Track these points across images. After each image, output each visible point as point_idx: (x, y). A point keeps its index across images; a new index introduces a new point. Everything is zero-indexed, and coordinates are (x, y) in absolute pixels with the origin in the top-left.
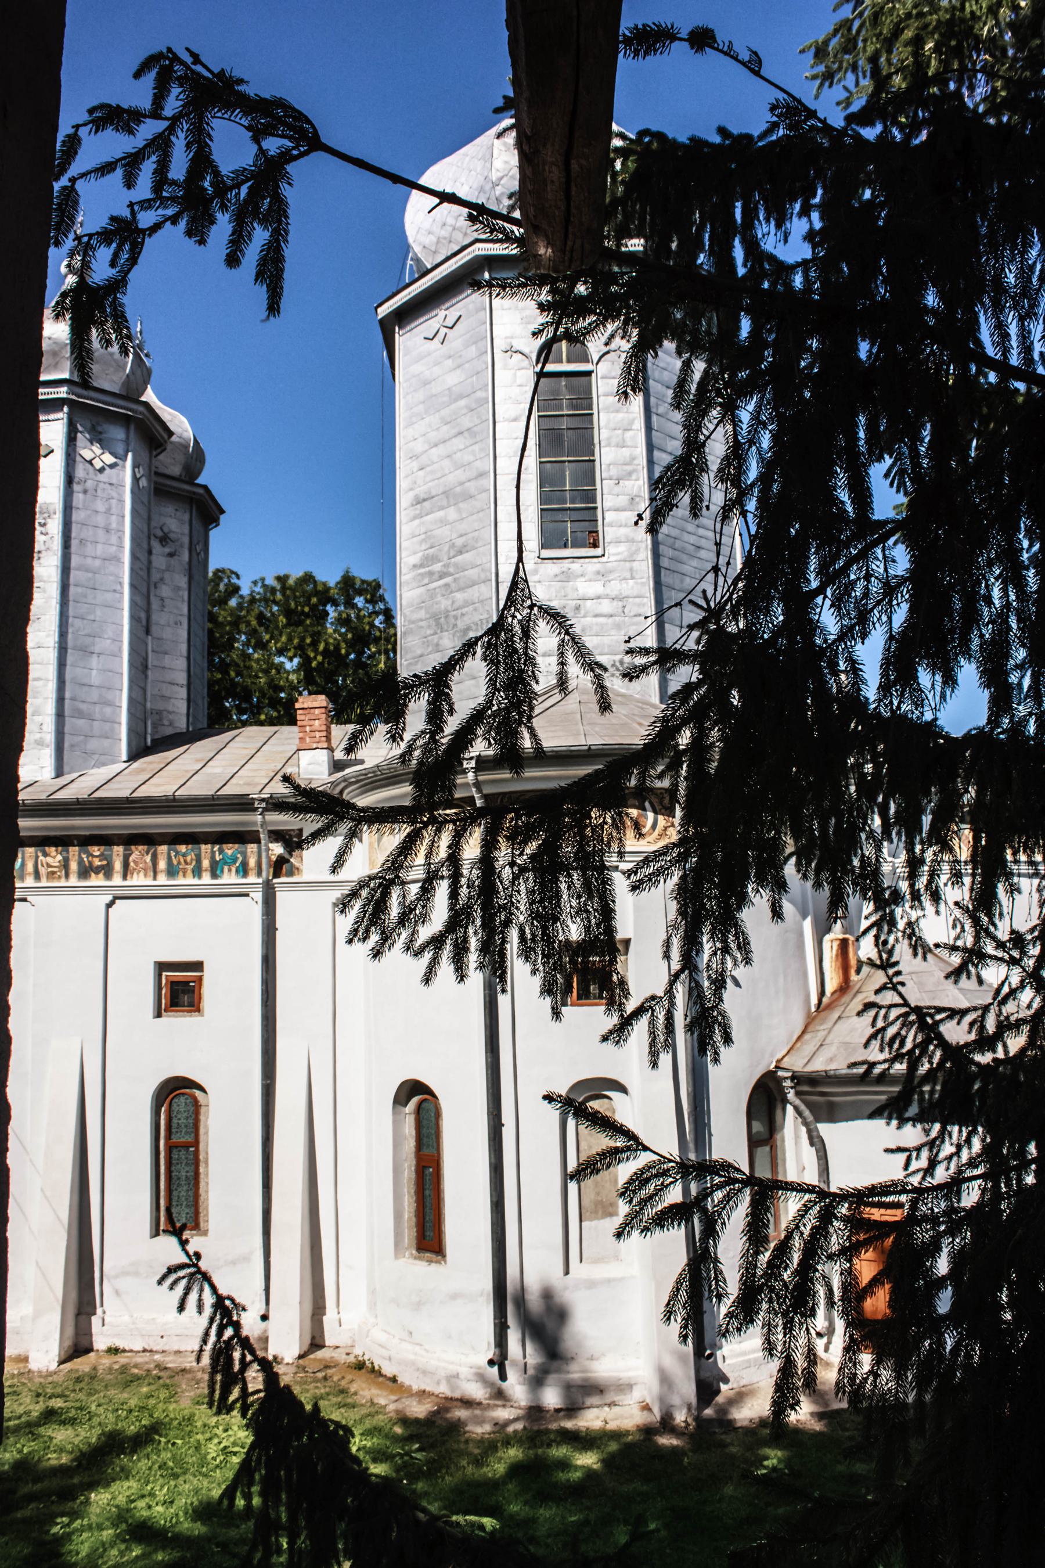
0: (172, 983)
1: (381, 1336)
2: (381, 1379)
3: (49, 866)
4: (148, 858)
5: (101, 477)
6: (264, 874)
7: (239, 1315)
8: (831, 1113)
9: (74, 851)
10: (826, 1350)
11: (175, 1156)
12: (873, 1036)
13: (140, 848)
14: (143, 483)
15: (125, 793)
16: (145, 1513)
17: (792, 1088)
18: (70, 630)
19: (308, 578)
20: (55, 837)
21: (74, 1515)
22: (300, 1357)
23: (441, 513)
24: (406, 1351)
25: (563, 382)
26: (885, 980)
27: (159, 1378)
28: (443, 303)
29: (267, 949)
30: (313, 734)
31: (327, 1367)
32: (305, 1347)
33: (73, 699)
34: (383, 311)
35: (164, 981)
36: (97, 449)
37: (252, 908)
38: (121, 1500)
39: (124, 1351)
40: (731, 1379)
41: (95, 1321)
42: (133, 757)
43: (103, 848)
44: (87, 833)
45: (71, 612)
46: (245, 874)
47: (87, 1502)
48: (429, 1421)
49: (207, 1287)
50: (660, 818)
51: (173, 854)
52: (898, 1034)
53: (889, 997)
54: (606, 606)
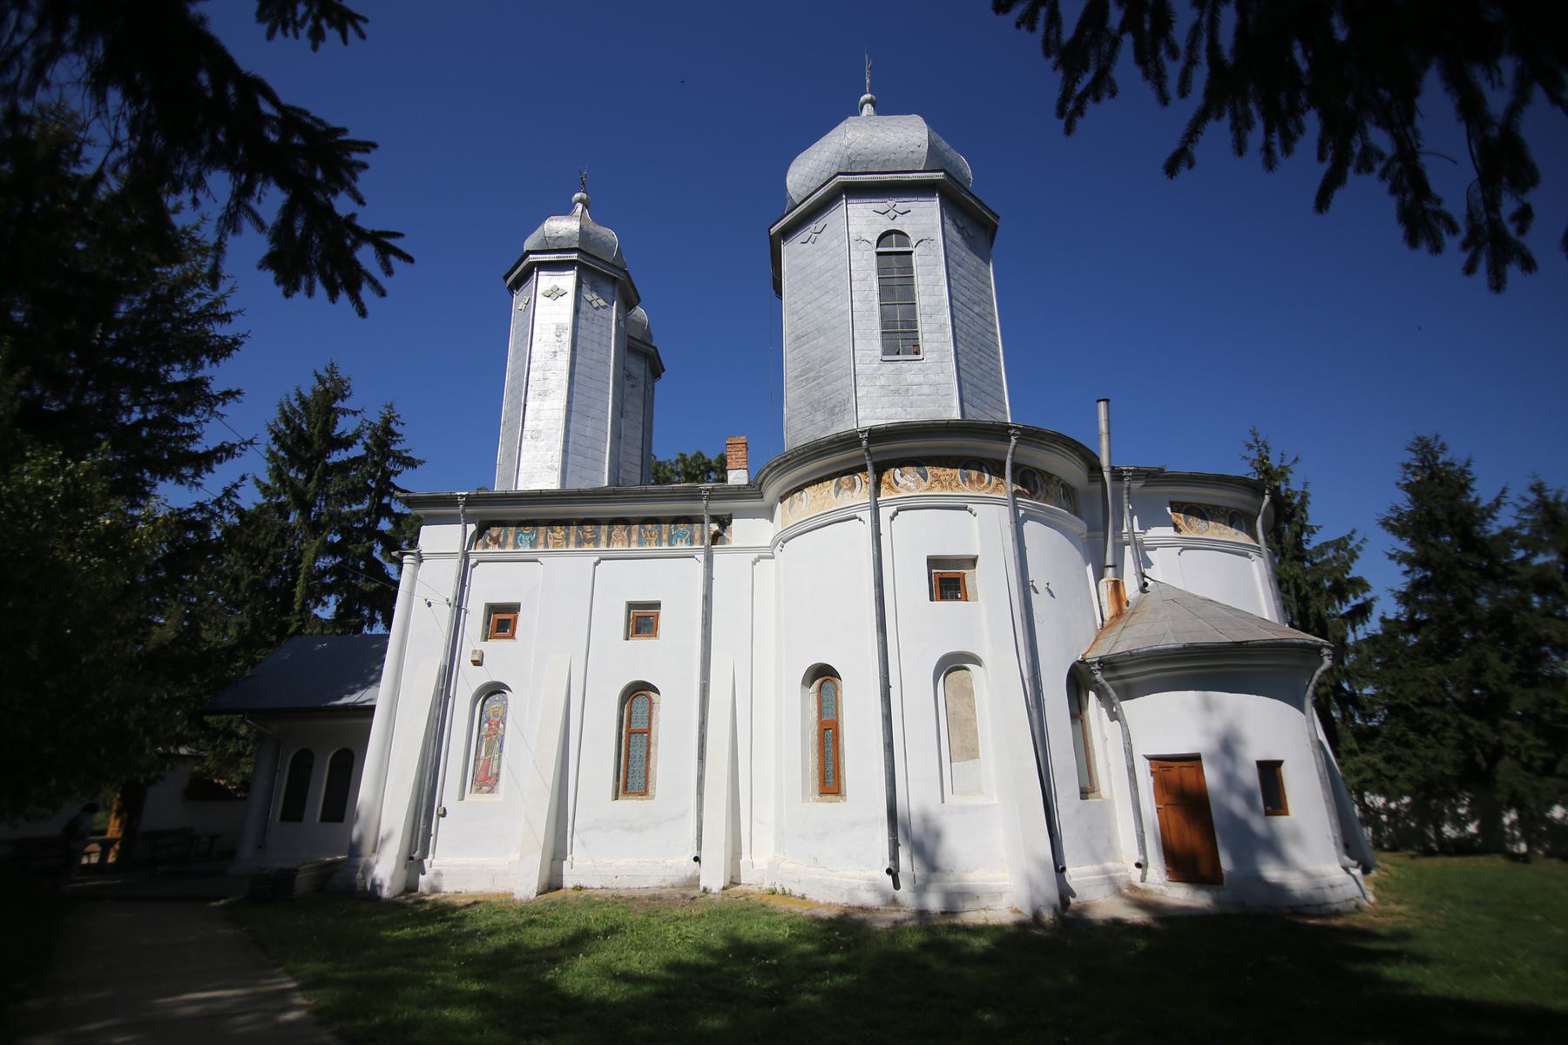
0: (637, 617)
2: (792, 898)
3: (555, 538)
4: (625, 534)
6: (706, 542)
8: (1129, 693)
9: (573, 529)
10: (1143, 879)
13: (620, 526)
17: (1099, 670)
18: (574, 400)
19: (700, 455)
20: (560, 520)
22: (724, 889)
23: (815, 341)
25: (894, 257)
27: (616, 903)
28: (814, 220)
29: (707, 590)
30: (737, 460)
33: (574, 443)
34: (773, 230)
35: (631, 616)
37: (697, 567)
39: (586, 888)
40: (1077, 894)
43: (594, 527)
44: (583, 517)
45: (575, 390)
46: (692, 543)
50: (993, 478)
51: (642, 530)
54: (925, 389)
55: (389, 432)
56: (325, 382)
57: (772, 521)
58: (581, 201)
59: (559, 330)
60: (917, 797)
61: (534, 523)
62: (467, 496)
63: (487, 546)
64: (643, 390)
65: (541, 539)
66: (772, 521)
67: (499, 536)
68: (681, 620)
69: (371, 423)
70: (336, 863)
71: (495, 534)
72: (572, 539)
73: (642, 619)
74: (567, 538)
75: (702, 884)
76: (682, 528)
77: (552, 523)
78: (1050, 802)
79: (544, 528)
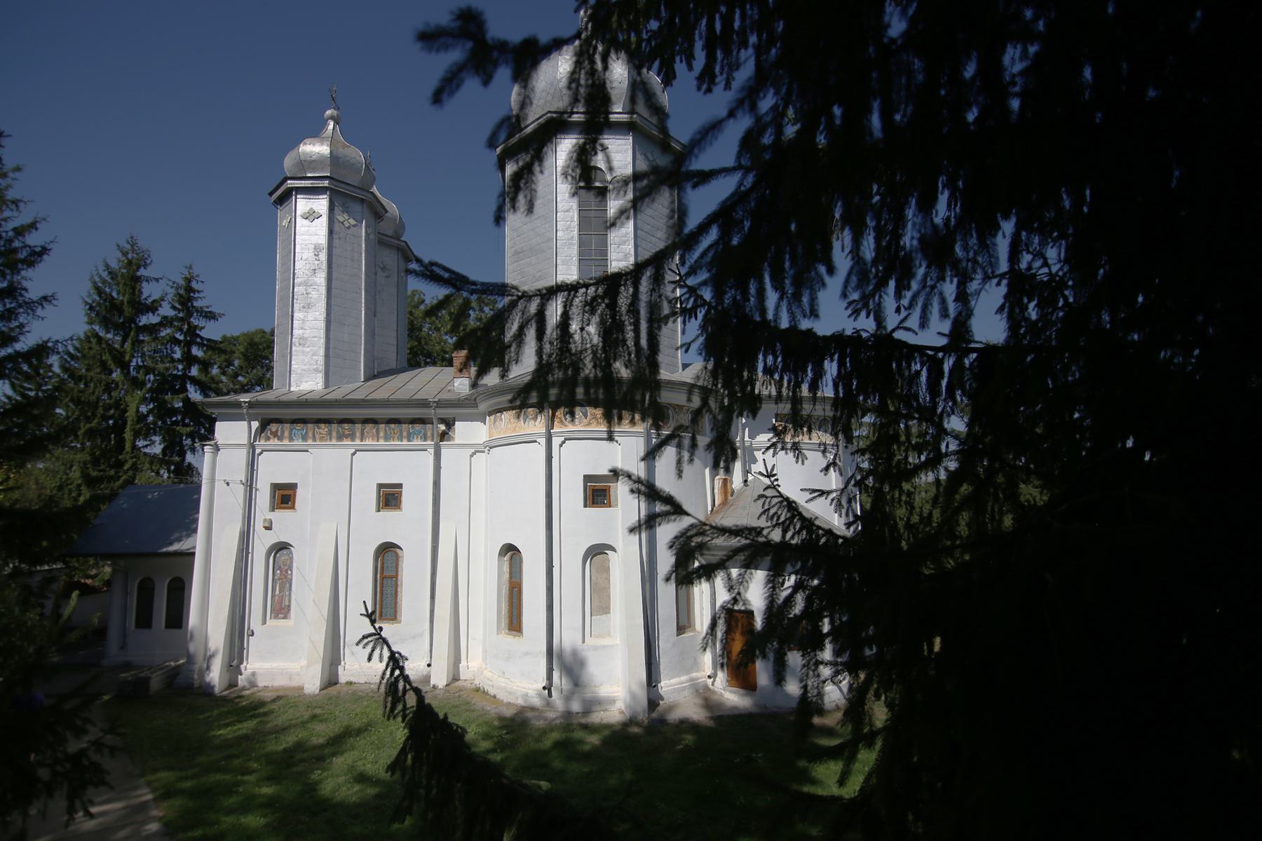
1: (487, 674)
3: (321, 434)
5: (349, 232)
7: (404, 663)
9: (334, 426)
10: (713, 685)
11: (385, 583)
12: (764, 512)
14: (372, 236)
15: (362, 397)
16: (362, 768)
18: (333, 312)
21: (324, 770)
22: (447, 685)
23: (528, 260)
24: (502, 682)
26: (770, 483)
31: (460, 690)
32: (450, 680)
36: (346, 216)
37: (429, 457)
38: (349, 761)
39: (355, 683)
41: (340, 668)
42: (368, 378)
47: (331, 763)
48: (512, 719)
49: (385, 647)
52: (776, 513)
53: (770, 493)
55: (190, 289)
56: (128, 253)
57: (485, 424)
58: (332, 118)
59: (317, 249)
60: (568, 637)
61: (304, 421)
62: (249, 402)
63: (268, 439)
64: (396, 279)
65: (310, 434)
66: (485, 424)
67: (277, 431)
68: (416, 498)
69: (174, 283)
70: (179, 666)
71: (274, 430)
72: (334, 434)
73: (390, 497)
74: (330, 433)
75: (432, 682)
76: (418, 427)
77: (318, 421)
78: (652, 644)
79: (311, 425)
